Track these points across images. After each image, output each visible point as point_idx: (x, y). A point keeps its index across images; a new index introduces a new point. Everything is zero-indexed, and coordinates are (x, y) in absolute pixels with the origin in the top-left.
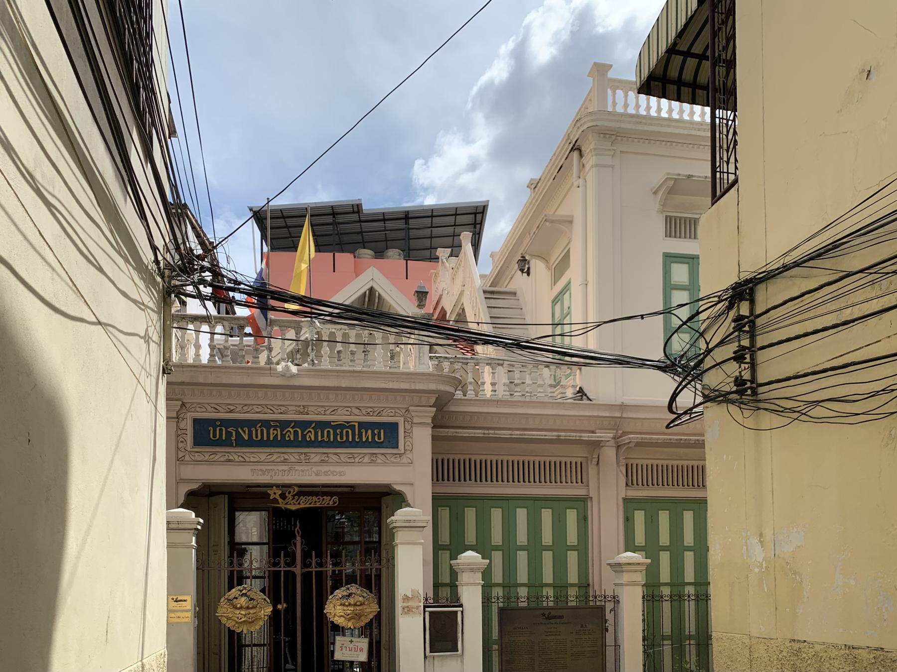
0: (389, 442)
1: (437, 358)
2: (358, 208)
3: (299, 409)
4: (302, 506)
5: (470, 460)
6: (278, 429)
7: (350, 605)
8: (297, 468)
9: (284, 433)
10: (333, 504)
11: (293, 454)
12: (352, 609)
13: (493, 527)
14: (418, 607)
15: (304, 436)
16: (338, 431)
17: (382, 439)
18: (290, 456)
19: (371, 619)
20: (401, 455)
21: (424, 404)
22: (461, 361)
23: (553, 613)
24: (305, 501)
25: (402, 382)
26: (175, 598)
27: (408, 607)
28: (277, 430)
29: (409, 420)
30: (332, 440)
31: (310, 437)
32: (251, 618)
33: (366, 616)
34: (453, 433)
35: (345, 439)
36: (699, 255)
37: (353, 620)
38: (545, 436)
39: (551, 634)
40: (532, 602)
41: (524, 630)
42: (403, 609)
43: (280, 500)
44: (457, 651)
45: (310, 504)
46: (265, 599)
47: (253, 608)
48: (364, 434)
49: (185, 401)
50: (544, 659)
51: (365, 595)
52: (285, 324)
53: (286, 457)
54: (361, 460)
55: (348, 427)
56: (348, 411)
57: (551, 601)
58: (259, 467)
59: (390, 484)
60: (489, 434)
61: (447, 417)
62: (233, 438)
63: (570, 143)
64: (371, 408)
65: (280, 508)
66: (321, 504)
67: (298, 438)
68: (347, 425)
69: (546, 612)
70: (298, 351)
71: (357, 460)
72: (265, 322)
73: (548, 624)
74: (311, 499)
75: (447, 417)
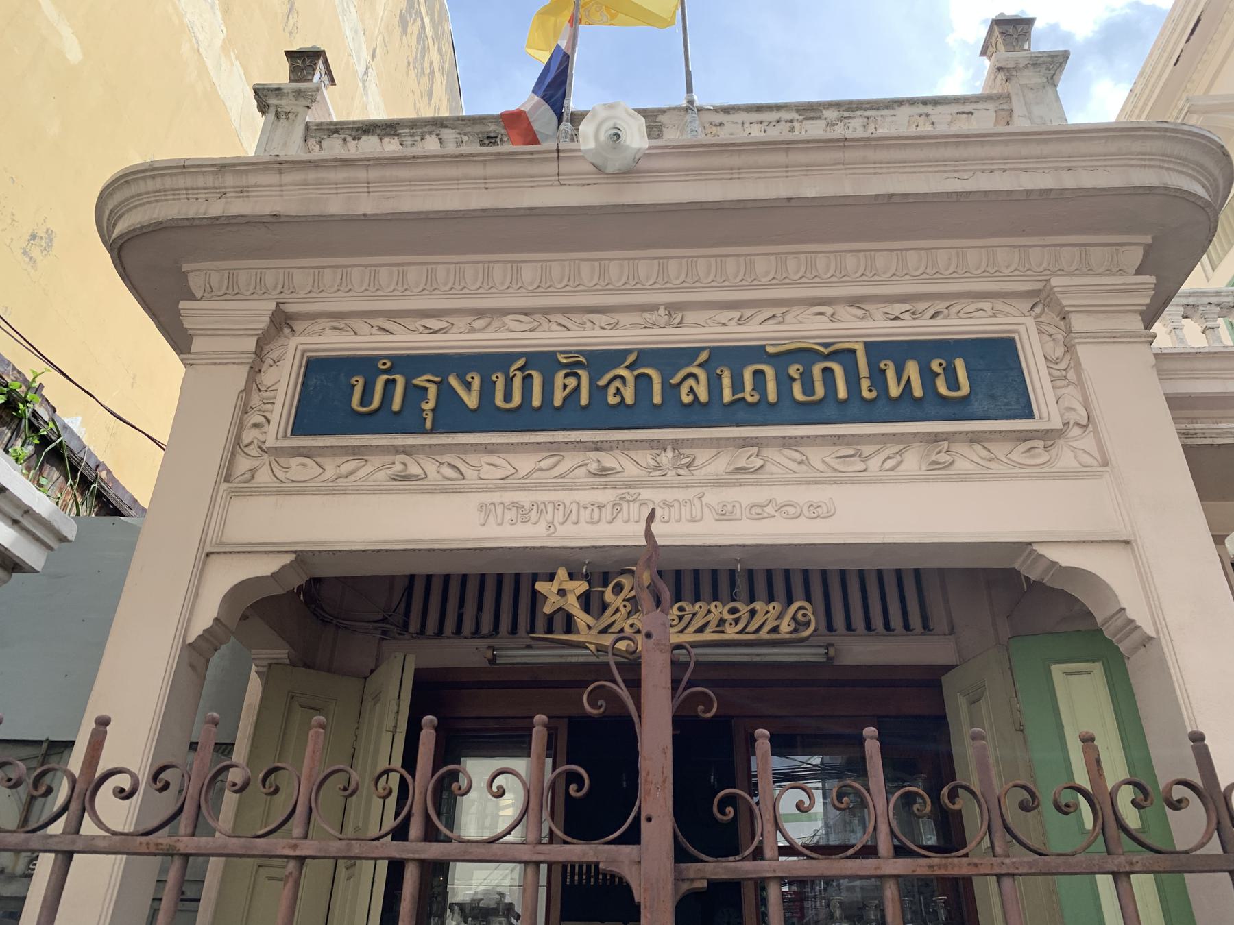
0: (992, 397)
10: (791, 633)
15: (671, 390)
16: (793, 370)
24: (681, 618)
25: (1025, 170)
28: (577, 375)
45: (700, 630)
48: (891, 375)
49: (290, 308)
59: (1030, 544)
62: (431, 405)
66: (741, 632)
74: (704, 611)
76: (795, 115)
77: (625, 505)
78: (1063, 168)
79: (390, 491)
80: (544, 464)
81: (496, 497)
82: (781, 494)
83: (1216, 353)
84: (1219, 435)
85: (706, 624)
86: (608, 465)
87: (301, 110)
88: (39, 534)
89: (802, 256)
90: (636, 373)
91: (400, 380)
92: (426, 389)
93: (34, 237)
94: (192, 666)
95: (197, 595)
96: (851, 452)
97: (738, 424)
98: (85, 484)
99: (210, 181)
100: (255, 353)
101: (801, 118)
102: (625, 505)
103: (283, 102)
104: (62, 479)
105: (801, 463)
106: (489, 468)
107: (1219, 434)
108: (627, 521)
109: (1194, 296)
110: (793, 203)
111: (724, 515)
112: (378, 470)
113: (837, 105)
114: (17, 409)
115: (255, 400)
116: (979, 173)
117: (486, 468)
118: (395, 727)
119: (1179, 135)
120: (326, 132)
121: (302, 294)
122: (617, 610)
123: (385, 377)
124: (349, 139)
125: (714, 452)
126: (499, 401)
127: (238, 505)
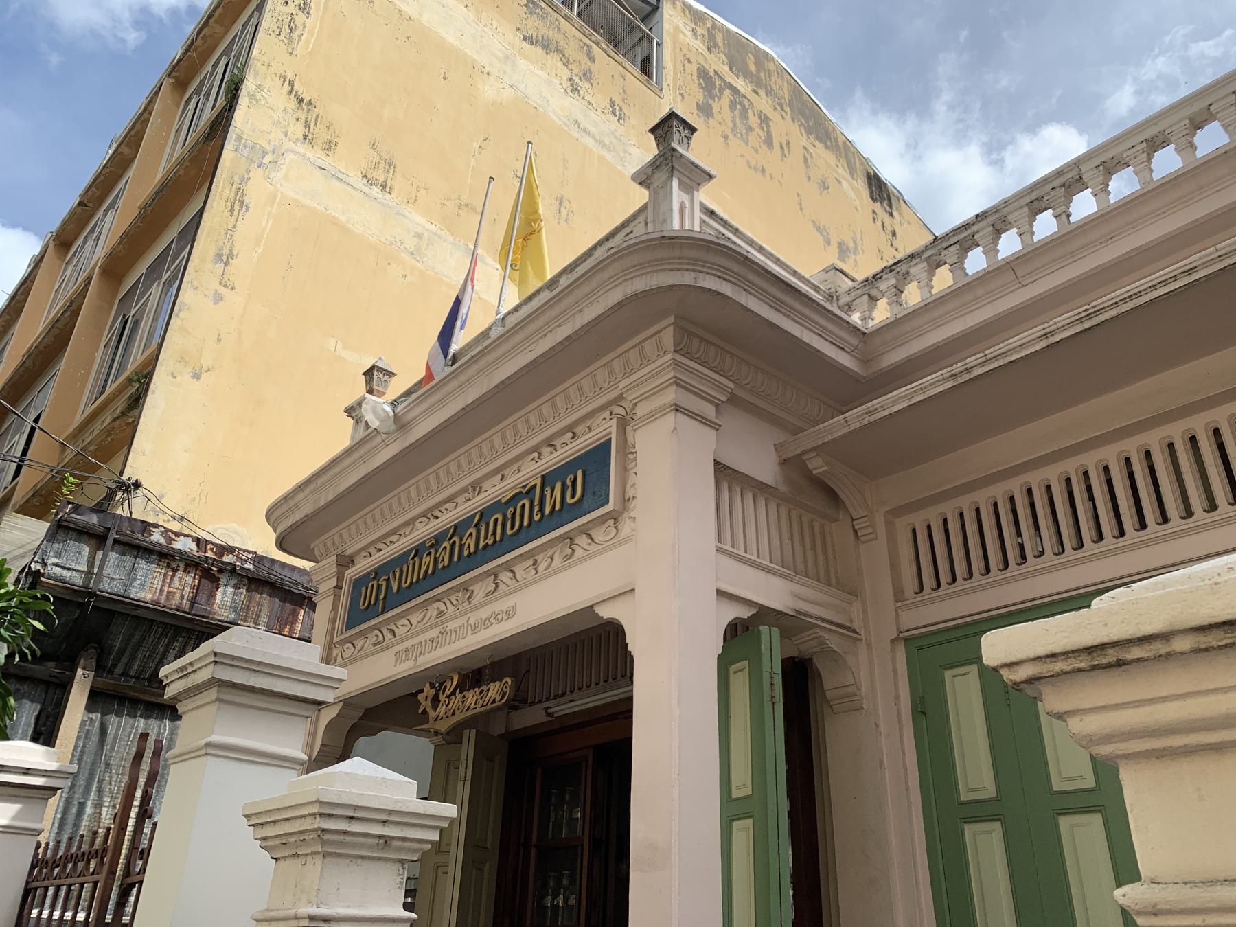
1: (891, 271)
30: (498, 538)
36: (54, 747)
38: (1188, 272)
59: (591, 607)
60: (969, 370)
63: (815, 146)
66: (482, 706)
79: (375, 653)
83: (942, 297)
84: (895, 402)
88: (291, 711)
107: (895, 401)
109: (1036, 189)
110: (468, 409)
116: (540, 341)
118: (465, 777)
119: (624, 252)
121: (348, 544)
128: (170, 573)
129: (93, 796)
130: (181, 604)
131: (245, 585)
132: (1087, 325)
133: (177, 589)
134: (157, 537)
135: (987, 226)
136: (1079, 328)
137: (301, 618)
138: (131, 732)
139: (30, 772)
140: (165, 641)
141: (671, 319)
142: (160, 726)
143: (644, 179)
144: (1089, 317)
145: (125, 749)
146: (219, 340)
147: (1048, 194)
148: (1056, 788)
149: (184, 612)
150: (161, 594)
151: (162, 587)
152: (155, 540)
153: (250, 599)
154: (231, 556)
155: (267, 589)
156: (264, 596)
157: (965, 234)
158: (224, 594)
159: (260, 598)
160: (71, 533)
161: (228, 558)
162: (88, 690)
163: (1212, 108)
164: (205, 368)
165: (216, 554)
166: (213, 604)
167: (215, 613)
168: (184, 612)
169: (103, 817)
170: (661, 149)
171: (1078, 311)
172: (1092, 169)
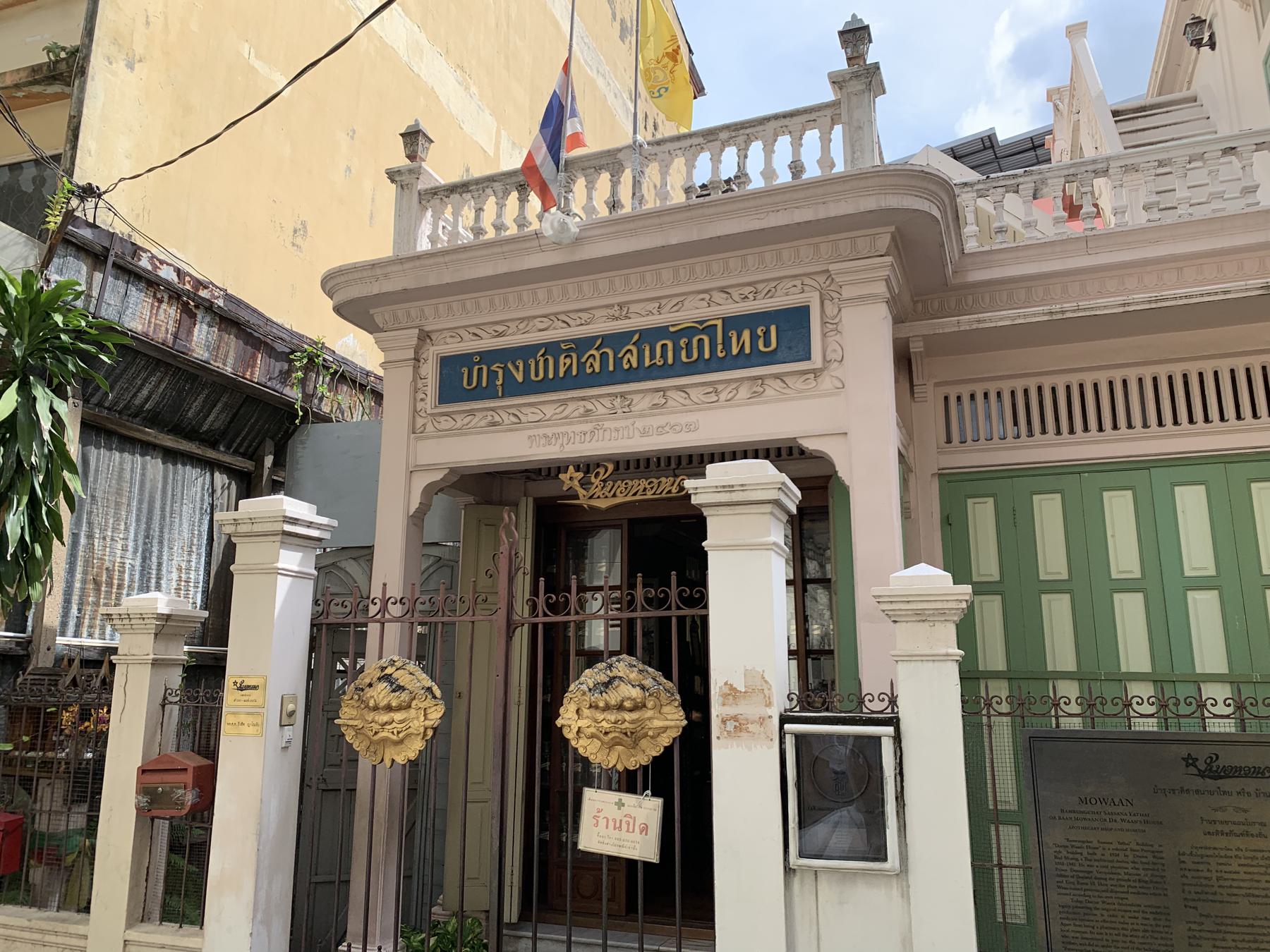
0: (790, 348)
2: (991, 141)
3: (611, 312)
4: (620, 499)
5: (1040, 389)
6: (573, 354)
7: (607, 708)
8: (607, 424)
9: (583, 360)
10: (678, 492)
11: (600, 399)
12: (613, 718)
13: (1113, 536)
14: (762, 720)
15: (618, 361)
16: (683, 342)
17: (774, 345)
18: (597, 404)
19: (666, 748)
20: (816, 373)
21: (865, 253)
22: (1003, 183)
23: (1228, 758)
24: (626, 488)
25: (797, 208)
26: (239, 681)
27: (735, 718)
28: (570, 357)
29: (835, 295)
30: (670, 361)
31: (629, 361)
32: (395, 733)
33: (652, 737)
34: (970, 322)
35: (695, 356)
37: (620, 748)
38: (1225, 292)
39: (1226, 829)
40: (1142, 716)
41: (1120, 809)
42: (724, 722)
43: (581, 492)
44: (885, 859)
45: (635, 494)
46: (429, 689)
47: (399, 708)
48: (734, 340)
49: (427, 328)
50: (1207, 916)
51: (648, 682)
52: (592, 162)
53: (590, 406)
54: (731, 395)
55: (703, 331)
56: (703, 299)
57: (1001, 714)
58: (541, 431)
59: (795, 438)
60: (1063, 312)
61: (970, 302)
62: (500, 382)
64: (749, 284)
65: (580, 506)
66: (654, 494)
67: (608, 367)
68: (701, 328)
69: (1202, 753)
70: (614, 206)
71: (723, 396)
72: (555, 168)
73: (1212, 793)
74: (637, 484)
75: (970, 302)
76: (701, 140)
77: (596, 432)
78: (819, 203)
80: (558, 411)
81: (535, 432)
82: (673, 419)
84: (1001, 319)
85: (637, 491)
86: (590, 408)
87: (414, 181)
89: (687, 266)
90: (601, 352)
91: (485, 368)
92: (497, 372)
93: (295, 231)
94: (415, 524)
95: (410, 492)
96: (711, 390)
97: (654, 379)
98: (362, 387)
99: (370, 273)
100: (415, 359)
101: (705, 142)
102: (596, 432)
103: (404, 178)
104: (349, 389)
105: (685, 398)
106: (530, 415)
108: (597, 441)
111: (644, 433)
112: (481, 420)
113: (727, 127)
114: (314, 361)
115: (420, 385)
116: (770, 213)
117: (530, 415)
120: (431, 195)
121: (431, 319)
122: (597, 487)
123: (477, 367)
124: (444, 198)
125: (643, 395)
126: (533, 377)
127: (421, 444)
128: (156, 304)
129: (84, 528)
130: (166, 337)
131: (217, 324)
132: (1154, 306)
133: (163, 321)
134: (144, 263)
135: (1031, 182)
136: (1147, 306)
137: (259, 362)
138: (109, 465)
139: (312, 525)
140: (143, 375)
141: (893, 229)
142: (133, 461)
143: (837, 81)
144: (1156, 301)
145: (106, 482)
146: (148, 23)
147: (1082, 174)
148: (1041, 578)
149: (168, 347)
150: (149, 326)
151: (150, 318)
152: (144, 266)
153: (220, 338)
154: (206, 291)
155: (234, 330)
156: (232, 336)
157: (1013, 182)
158: (200, 331)
159: (228, 339)
160: (70, 248)
161: (203, 293)
162: (80, 420)
163: (1205, 155)
164: (137, 57)
165: (193, 287)
166: (192, 341)
167: (193, 351)
168: (168, 347)
169: (96, 548)
170: (849, 50)
171: (1151, 295)
172: (1117, 168)
